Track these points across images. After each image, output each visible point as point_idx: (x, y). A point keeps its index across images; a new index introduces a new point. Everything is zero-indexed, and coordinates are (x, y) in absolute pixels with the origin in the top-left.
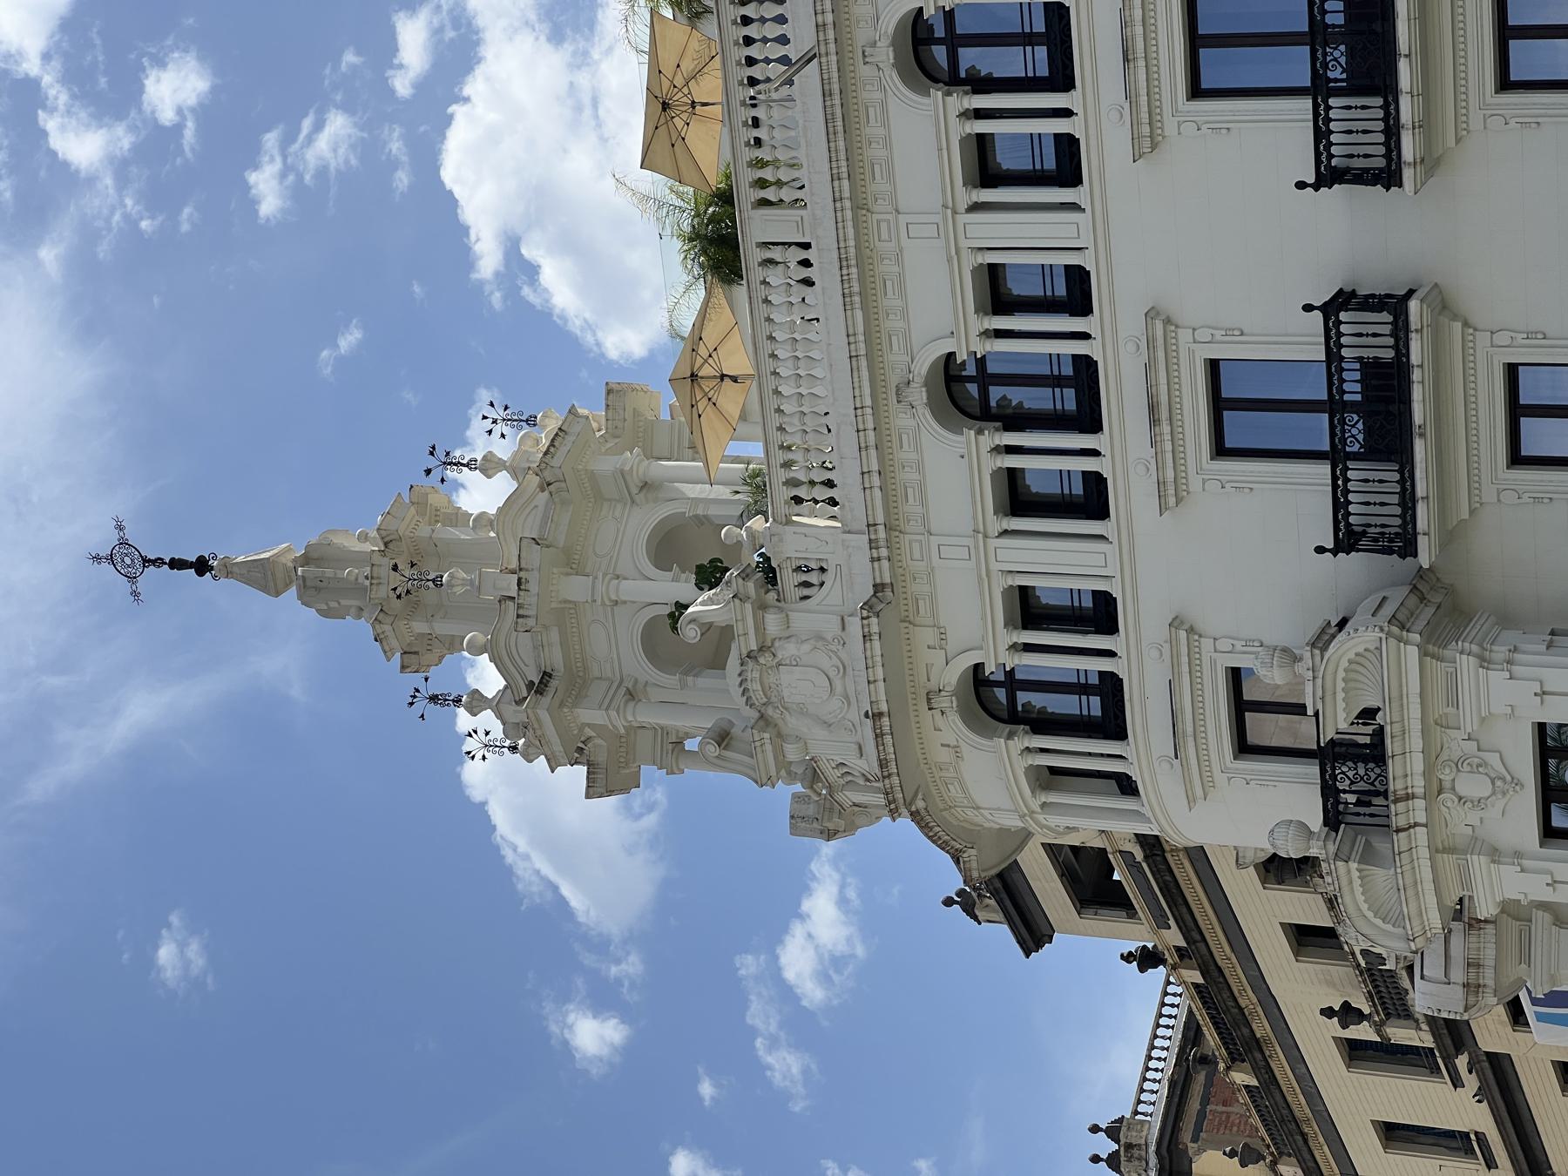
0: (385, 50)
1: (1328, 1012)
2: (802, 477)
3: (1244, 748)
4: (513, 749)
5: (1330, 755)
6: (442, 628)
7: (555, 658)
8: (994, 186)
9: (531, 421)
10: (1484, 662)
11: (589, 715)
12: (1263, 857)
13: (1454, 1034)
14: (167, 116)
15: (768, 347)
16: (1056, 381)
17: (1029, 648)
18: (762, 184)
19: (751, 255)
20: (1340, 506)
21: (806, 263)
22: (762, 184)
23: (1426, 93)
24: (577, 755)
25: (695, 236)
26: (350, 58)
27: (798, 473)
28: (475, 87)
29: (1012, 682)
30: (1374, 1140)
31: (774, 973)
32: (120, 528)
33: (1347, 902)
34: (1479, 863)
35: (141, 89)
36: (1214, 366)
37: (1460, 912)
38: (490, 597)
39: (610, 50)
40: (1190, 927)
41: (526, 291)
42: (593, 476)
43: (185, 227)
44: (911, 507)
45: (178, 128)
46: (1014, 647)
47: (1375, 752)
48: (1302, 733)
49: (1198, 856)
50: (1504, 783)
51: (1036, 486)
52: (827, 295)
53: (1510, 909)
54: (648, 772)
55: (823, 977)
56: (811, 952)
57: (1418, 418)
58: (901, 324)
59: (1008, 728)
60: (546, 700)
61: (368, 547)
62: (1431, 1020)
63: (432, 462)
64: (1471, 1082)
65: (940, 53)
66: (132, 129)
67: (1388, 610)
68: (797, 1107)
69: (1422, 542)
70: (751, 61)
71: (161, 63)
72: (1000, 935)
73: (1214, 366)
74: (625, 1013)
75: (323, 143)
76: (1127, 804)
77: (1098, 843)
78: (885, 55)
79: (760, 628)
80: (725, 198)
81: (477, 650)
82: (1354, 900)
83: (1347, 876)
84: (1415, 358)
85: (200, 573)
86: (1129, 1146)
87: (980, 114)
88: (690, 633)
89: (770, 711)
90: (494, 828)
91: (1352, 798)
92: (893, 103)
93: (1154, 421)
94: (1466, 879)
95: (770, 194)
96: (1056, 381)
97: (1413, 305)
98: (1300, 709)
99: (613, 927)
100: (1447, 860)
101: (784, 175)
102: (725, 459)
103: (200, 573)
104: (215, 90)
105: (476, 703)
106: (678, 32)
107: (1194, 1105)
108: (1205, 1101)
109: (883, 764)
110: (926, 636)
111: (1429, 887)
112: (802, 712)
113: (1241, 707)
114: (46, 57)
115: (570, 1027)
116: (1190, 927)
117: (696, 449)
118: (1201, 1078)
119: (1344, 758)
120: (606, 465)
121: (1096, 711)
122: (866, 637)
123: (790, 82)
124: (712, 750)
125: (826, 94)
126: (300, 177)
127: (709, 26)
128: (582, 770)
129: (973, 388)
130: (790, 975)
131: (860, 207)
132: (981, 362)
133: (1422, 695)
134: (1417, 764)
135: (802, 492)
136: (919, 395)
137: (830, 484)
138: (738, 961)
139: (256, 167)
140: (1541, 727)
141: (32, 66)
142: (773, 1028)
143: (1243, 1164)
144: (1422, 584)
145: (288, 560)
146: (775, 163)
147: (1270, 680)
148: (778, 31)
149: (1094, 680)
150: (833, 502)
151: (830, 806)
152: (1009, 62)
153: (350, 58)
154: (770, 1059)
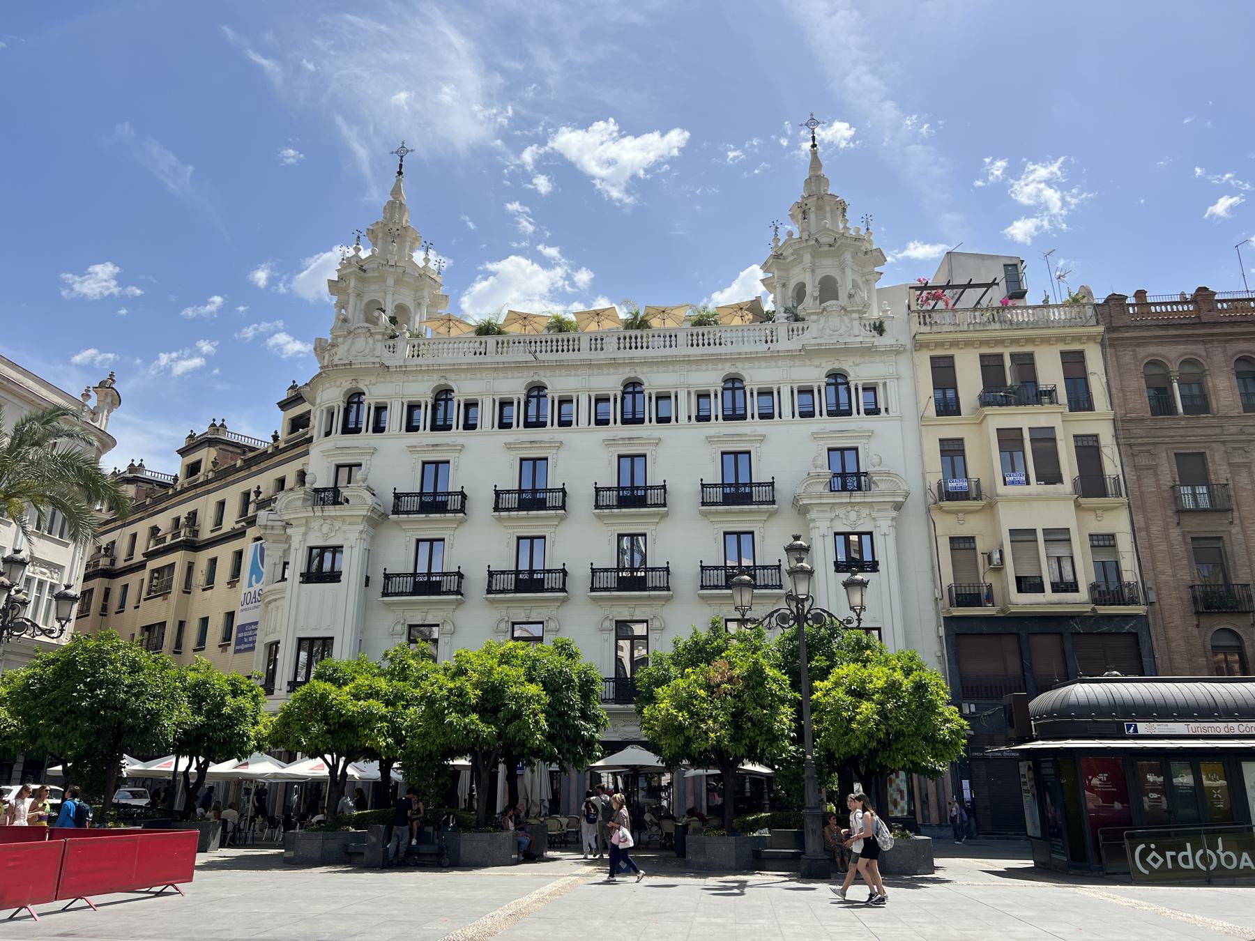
0: (550, 244)
1: (259, 487)
2: (420, 348)
3: (338, 467)
4: (343, 259)
5: (336, 490)
6: (380, 242)
7: (370, 274)
8: (432, 409)
9: (439, 273)
10: (361, 532)
11: (353, 283)
12: (306, 471)
13: (252, 522)
14: (535, 181)
15: (458, 341)
16: (445, 420)
17: (369, 408)
18: (503, 343)
19: (483, 338)
20: (407, 495)
21: (480, 354)
22: (503, 343)
23: (518, 518)
24: (341, 278)
25: (489, 323)
26: (548, 234)
27: (422, 347)
28: (536, 267)
29: (359, 403)
30: (220, 499)
31: (279, 331)
32: (412, 151)
33: (291, 494)
34: (303, 529)
35: (542, 174)
36: (448, 462)
37: (288, 524)
38: (388, 256)
39: (544, 305)
40: (285, 450)
41: (480, 276)
42: (423, 289)
43: (504, 182)
44: (596, 371)
45: (531, 184)
46: (553, 398)
47: (336, 502)
48: (342, 482)
49: (306, 453)
50: (326, 536)
51: (416, 413)
52: (471, 358)
53: (289, 538)
54: (335, 299)
55: (276, 345)
56: (283, 342)
57: (431, 515)
58: (605, 372)
59: (346, 401)
60: (357, 270)
61: (404, 222)
62: (256, 516)
63: (428, 243)
64: (239, 526)
65: (535, 393)
66: (532, 171)
67: (377, 507)
68: (236, 335)
69: (397, 516)
70: (536, 342)
71: (549, 180)
72: (284, 396)
73: (448, 462)
74: (268, 287)
75: (526, 224)
76: (323, 433)
77: (311, 425)
78: (536, 378)
79: (854, 311)
80: (500, 333)
81: (373, 251)
82: (292, 496)
83: (300, 493)
84: (447, 515)
85: (398, 172)
86: (218, 430)
87: (519, 403)
88: (376, 313)
89: (353, 334)
90: (325, 253)
91: (322, 496)
92: (523, 380)
93: (433, 446)
94: (298, 526)
95: (500, 345)
96: (445, 420)
97: (462, 515)
98: (349, 482)
99: (294, 285)
100: (304, 521)
101: (505, 349)
102: (426, 327)
103: (398, 172)
104: (541, 195)
105: (358, 250)
106: (545, 323)
107: (231, 449)
108: (232, 452)
109: (336, 365)
110: (374, 380)
111: (296, 516)
112: (353, 343)
113: (350, 466)
114: (553, 149)
115: (263, 270)
116: (285, 450)
117: (429, 319)
118: (239, 451)
119: (335, 494)
120: (426, 293)
121: (438, 423)
122: (374, 363)
123: (530, 352)
124: (342, 317)
125: (526, 362)
126: (517, 216)
127: (546, 332)
128: (336, 279)
129: (444, 397)
130: (277, 336)
131: (495, 369)
132: (451, 399)
133: (821, 504)
134: (332, 514)
135: (416, 348)
136: (443, 382)
137: (418, 356)
138: (281, 321)
139: (520, 204)
140: (342, 547)
141: (550, 144)
142: (261, 330)
143: (212, 462)
144: (384, 516)
145: (401, 198)
146: (508, 347)
147: (358, 474)
148: (544, 350)
149: (359, 426)
150: (413, 356)
151: (324, 350)
152: (532, 411)
153: (548, 234)
154: (251, 328)
